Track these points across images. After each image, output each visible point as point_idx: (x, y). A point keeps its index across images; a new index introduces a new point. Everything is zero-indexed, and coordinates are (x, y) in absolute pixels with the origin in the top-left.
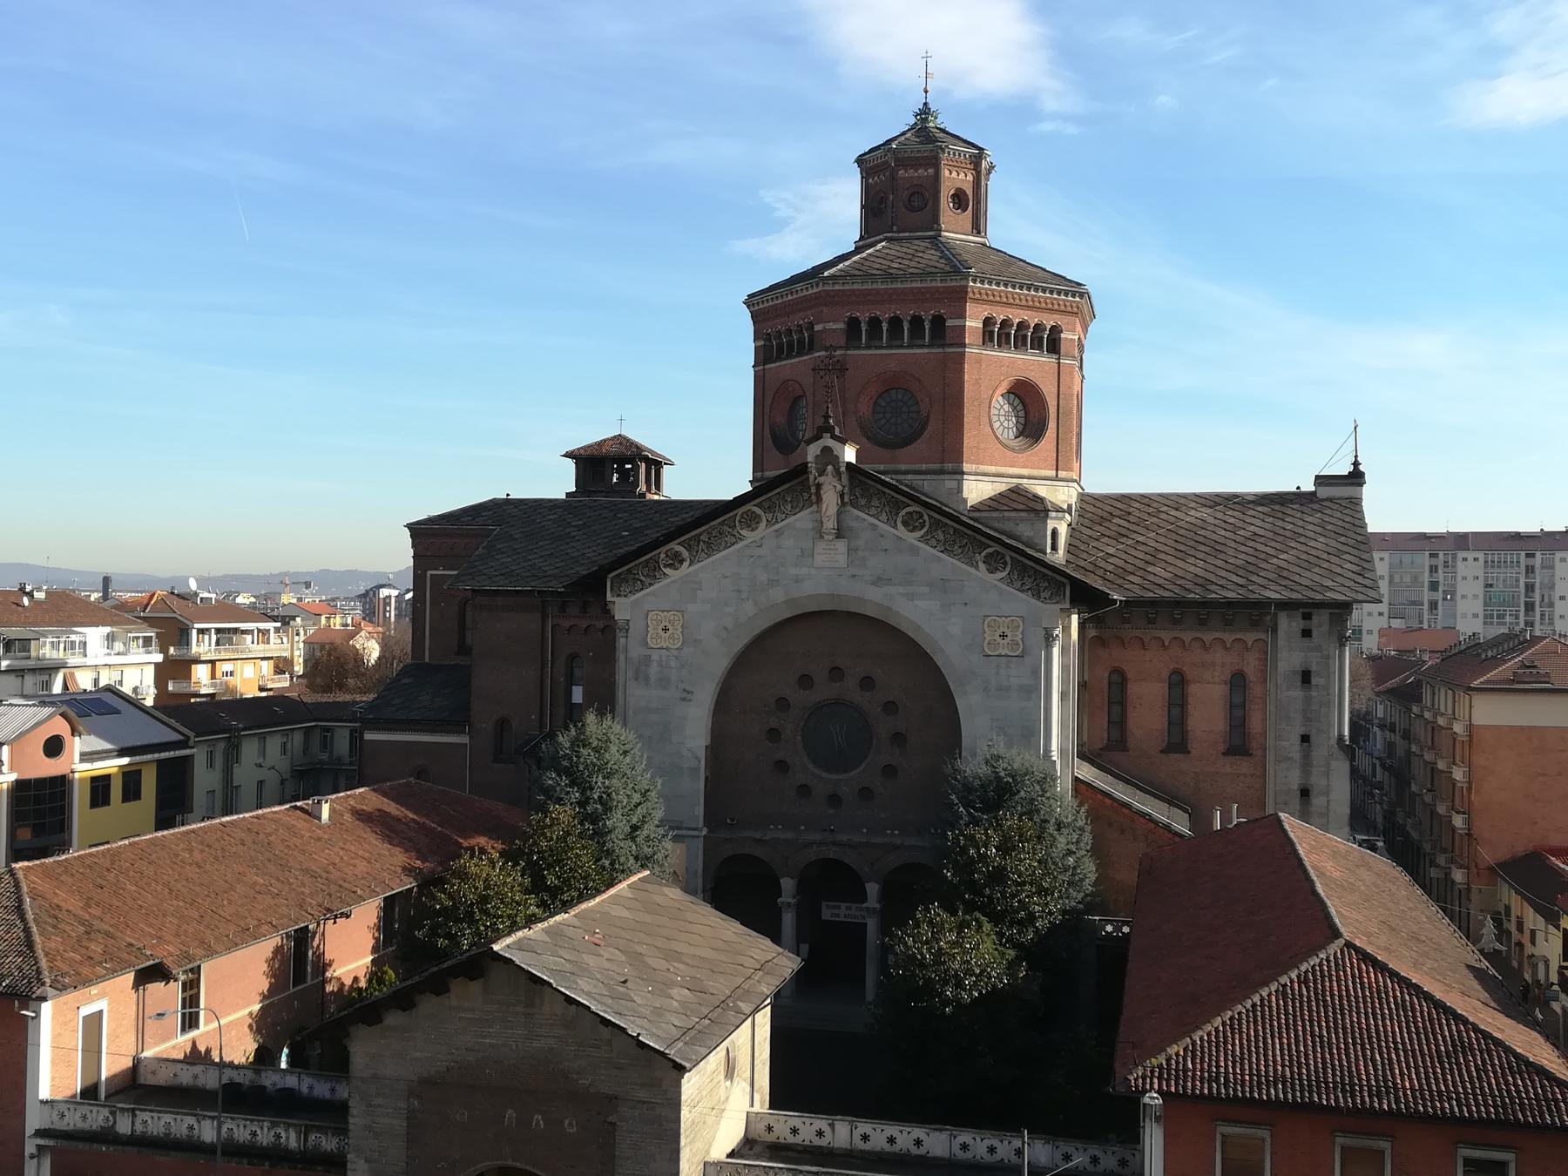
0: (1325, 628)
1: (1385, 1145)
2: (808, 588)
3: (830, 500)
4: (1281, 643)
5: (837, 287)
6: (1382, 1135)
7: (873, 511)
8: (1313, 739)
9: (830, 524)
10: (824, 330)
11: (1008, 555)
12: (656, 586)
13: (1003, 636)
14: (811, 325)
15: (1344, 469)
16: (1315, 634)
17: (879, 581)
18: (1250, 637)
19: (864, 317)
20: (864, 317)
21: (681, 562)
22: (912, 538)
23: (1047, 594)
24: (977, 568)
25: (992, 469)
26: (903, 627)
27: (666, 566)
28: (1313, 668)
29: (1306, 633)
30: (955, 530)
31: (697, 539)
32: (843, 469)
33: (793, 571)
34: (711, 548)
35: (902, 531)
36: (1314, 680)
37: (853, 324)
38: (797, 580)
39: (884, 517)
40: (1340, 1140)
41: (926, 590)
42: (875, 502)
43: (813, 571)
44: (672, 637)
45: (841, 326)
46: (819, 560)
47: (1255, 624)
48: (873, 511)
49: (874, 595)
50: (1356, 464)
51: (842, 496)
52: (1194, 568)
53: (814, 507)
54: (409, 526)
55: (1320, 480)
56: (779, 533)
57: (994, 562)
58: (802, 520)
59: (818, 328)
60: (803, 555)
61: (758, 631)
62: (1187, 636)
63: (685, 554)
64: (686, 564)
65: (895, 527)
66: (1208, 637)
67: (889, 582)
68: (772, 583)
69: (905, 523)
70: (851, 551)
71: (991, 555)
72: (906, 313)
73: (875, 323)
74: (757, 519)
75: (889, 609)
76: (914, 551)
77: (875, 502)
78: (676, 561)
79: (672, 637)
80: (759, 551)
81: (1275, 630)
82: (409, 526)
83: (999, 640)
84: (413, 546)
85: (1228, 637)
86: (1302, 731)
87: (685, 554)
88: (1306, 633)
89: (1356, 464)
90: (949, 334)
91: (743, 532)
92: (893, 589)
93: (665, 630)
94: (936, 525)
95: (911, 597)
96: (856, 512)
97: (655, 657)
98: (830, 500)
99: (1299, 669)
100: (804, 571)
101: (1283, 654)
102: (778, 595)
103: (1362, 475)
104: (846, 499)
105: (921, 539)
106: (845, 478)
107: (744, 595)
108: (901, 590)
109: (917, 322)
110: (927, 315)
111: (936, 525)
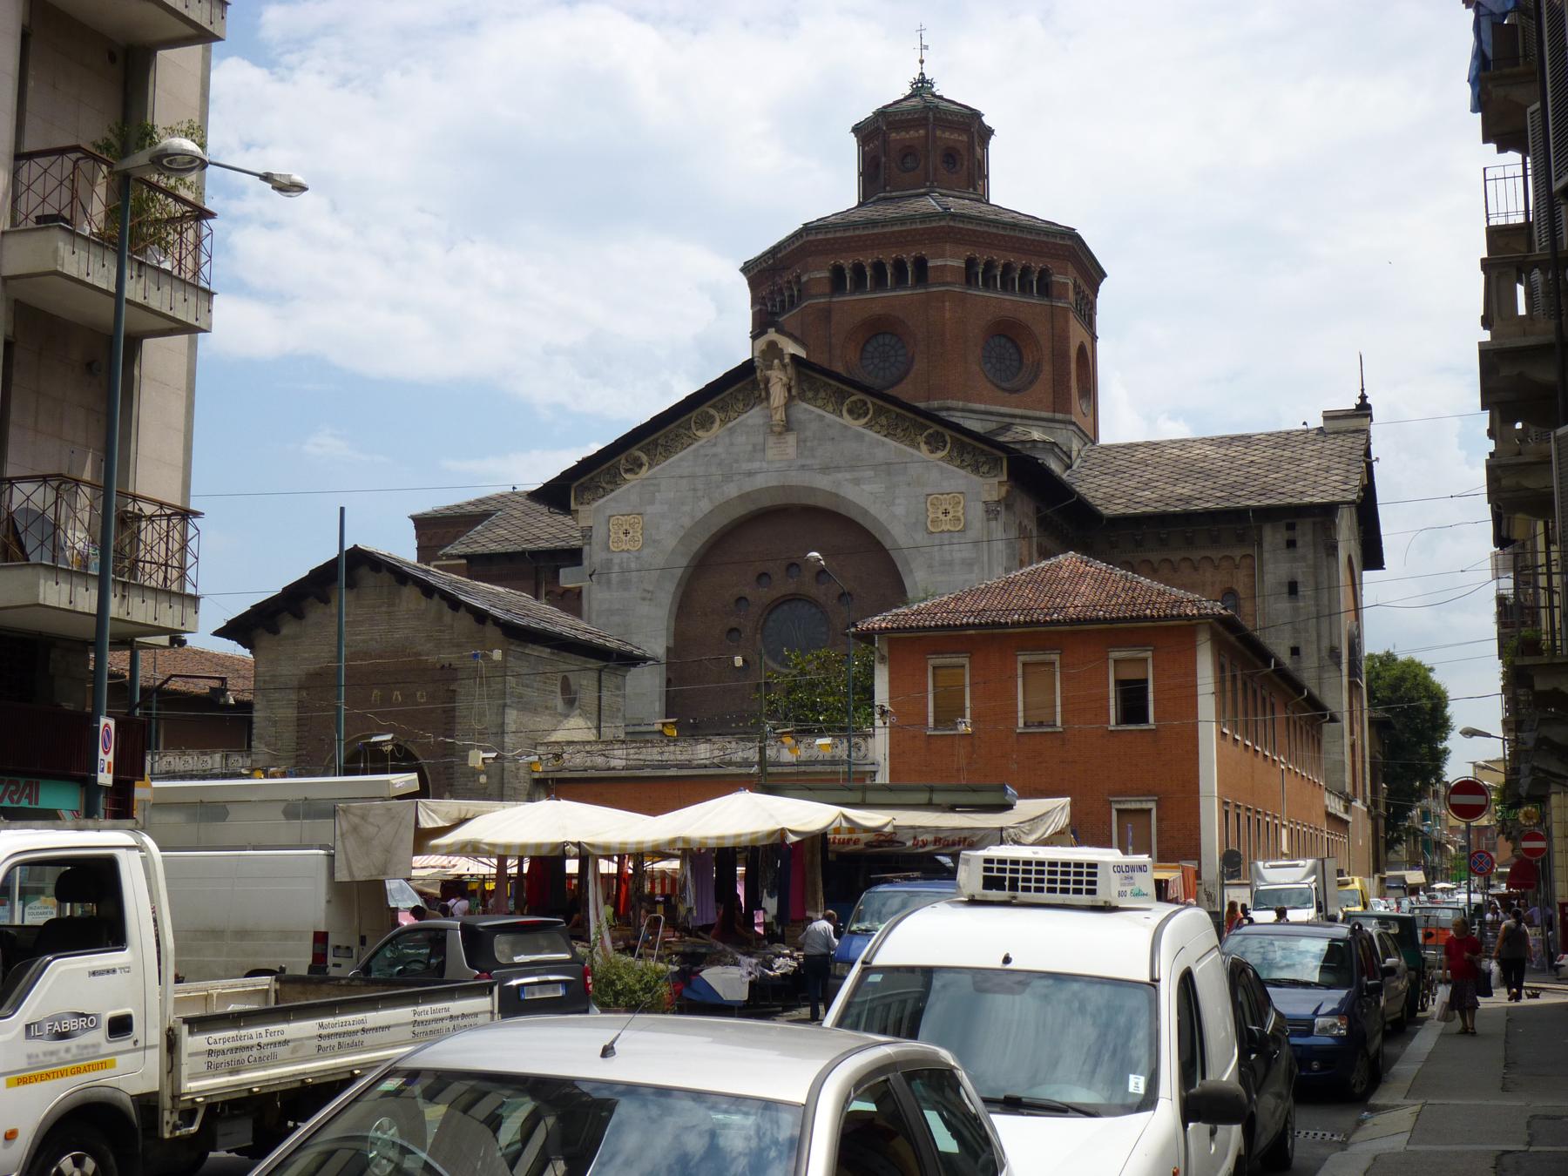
0: (1309, 538)
1: (1056, 657)
2: (760, 482)
3: (778, 394)
4: (1266, 555)
5: (820, 237)
6: (1052, 649)
7: (820, 402)
8: (1303, 652)
9: (779, 416)
10: (810, 280)
11: (948, 434)
12: (617, 492)
13: (946, 513)
14: (799, 277)
15: (1351, 403)
16: (1299, 544)
17: (825, 469)
18: (1237, 553)
19: (847, 263)
20: (847, 263)
21: (641, 466)
22: (857, 425)
23: (985, 468)
24: (918, 448)
25: (982, 407)
26: (853, 514)
27: (627, 471)
28: (1300, 579)
29: (1291, 544)
30: (898, 415)
31: (655, 444)
32: (787, 360)
33: (746, 466)
34: (668, 451)
35: (847, 420)
36: (1301, 589)
37: (838, 272)
38: (750, 474)
39: (830, 407)
40: (1021, 658)
41: (871, 473)
42: (822, 394)
43: (765, 465)
44: (633, 540)
45: (825, 274)
46: (771, 454)
47: (1241, 539)
48: (820, 402)
49: (823, 482)
50: (1363, 397)
51: (789, 390)
52: (1184, 490)
53: (765, 404)
54: (414, 518)
55: (1329, 416)
56: (732, 431)
57: (935, 443)
58: (754, 416)
59: (804, 279)
60: (755, 450)
61: (714, 530)
62: (1176, 557)
63: (644, 458)
64: (645, 468)
65: (841, 416)
66: (1196, 555)
67: (838, 468)
68: (727, 478)
69: (850, 412)
70: (801, 442)
71: (931, 435)
72: (888, 257)
73: (859, 270)
74: (711, 420)
75: (837, 495)
76: (859, 437)
77: (822, 394)
78: (636, 466)
79: (633, 540)
80: (714, 450)
81: (1260, 545)
82: (414, 518)
83: (942, 517)
84: (418, 537)
85: (1215, 554)
86: (1291, 643)
87: (644, 458)
88: (1291, 544)
89: (1363, 397)
90: (931, 274)
91: (699, 433)
92: (840, 476)
93: (626, 533)
94: (879, 412)
95: (857, 482)
96: (805, 405)
97: (616, 561)
98: (778, 394)
99: (1286, 580)
100: (756, 465)
101: (1269, 568)
102: (732, 491)
103: (1369, 407)
104: (794, 392)
105: (866, 426)
106: (790, 370)
107: (700, 494)
108: (848, 476)
109: (900, 266)
110: (908, 256)
111: (879, 412)
